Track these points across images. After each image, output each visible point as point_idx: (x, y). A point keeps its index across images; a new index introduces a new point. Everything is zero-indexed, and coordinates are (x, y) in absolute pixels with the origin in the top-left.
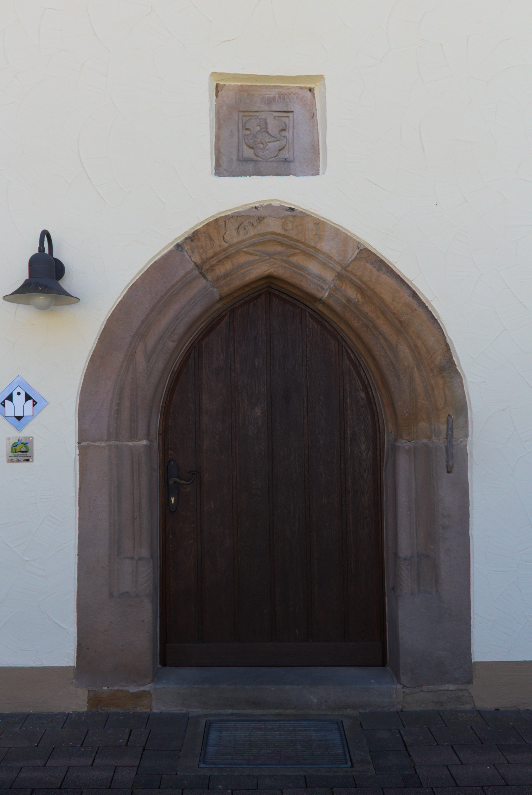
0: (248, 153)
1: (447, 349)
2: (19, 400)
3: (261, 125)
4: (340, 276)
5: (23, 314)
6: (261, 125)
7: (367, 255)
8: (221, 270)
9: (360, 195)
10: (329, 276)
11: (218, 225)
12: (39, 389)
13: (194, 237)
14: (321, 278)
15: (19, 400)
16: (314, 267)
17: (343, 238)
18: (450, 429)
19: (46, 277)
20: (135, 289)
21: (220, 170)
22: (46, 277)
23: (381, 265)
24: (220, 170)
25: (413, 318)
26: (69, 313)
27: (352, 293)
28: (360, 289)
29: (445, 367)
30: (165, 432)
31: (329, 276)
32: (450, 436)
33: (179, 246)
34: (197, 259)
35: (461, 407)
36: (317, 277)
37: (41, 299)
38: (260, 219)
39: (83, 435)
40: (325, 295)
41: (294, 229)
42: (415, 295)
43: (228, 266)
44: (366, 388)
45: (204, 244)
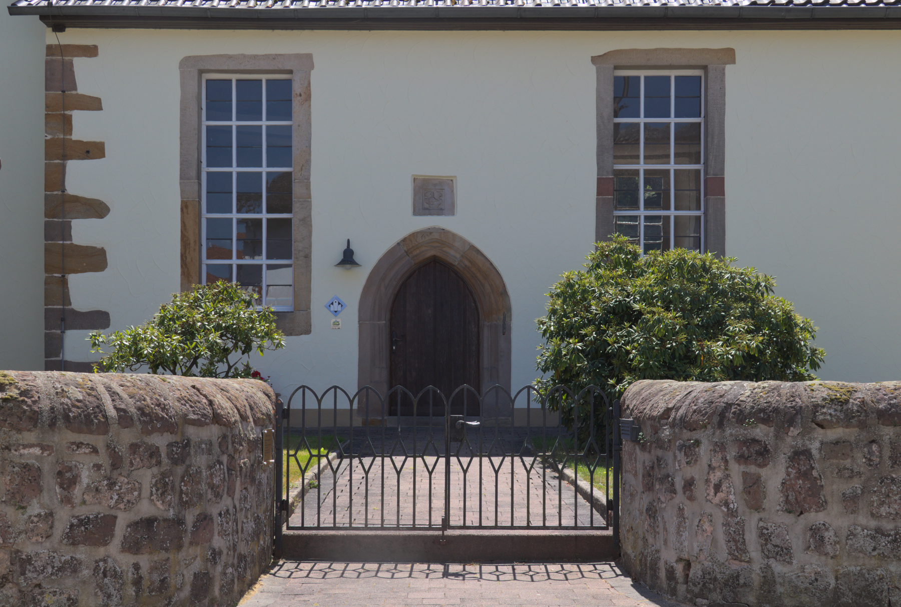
0: (426, 206)
1: (504, 286)
2: (336, 304)
3: (432, 195)
4: (462, 256)
5: (340, 270)
6: (432, 195)
7: (473, 248)
8: (415, 253)
9: (471, 224)
10: (458, 256)
11: (414, 235)
12: (344, 300)
13: (404, 240)
14: (19, 431)
15: (336, 304)
16: (452, 252)
17: (463, 241)
18: (505, 318)
19: (348, 259)
20: (381, 261)
21: (415, 213)
22: (348, 259)
23: (479, 252)
24: (415, 213)
25: (491, 273)
26: (356, 270)
27: (467, 263)
28: (470, 261)
29: (503, 293)
30: (391, 319)
31: (458, 256)
32: (504, 320)
33: (398, 244)
34: (406, 249)
35: (509, 309)
36: (453, 256)
37: (348, 266)
38: (431, 233)
39: (361, 319)
40: (456, 263)
41: (444, 237)
42: (491, 264)
43: (418, 251)
44: (475, 302)
45: (408, 243)
